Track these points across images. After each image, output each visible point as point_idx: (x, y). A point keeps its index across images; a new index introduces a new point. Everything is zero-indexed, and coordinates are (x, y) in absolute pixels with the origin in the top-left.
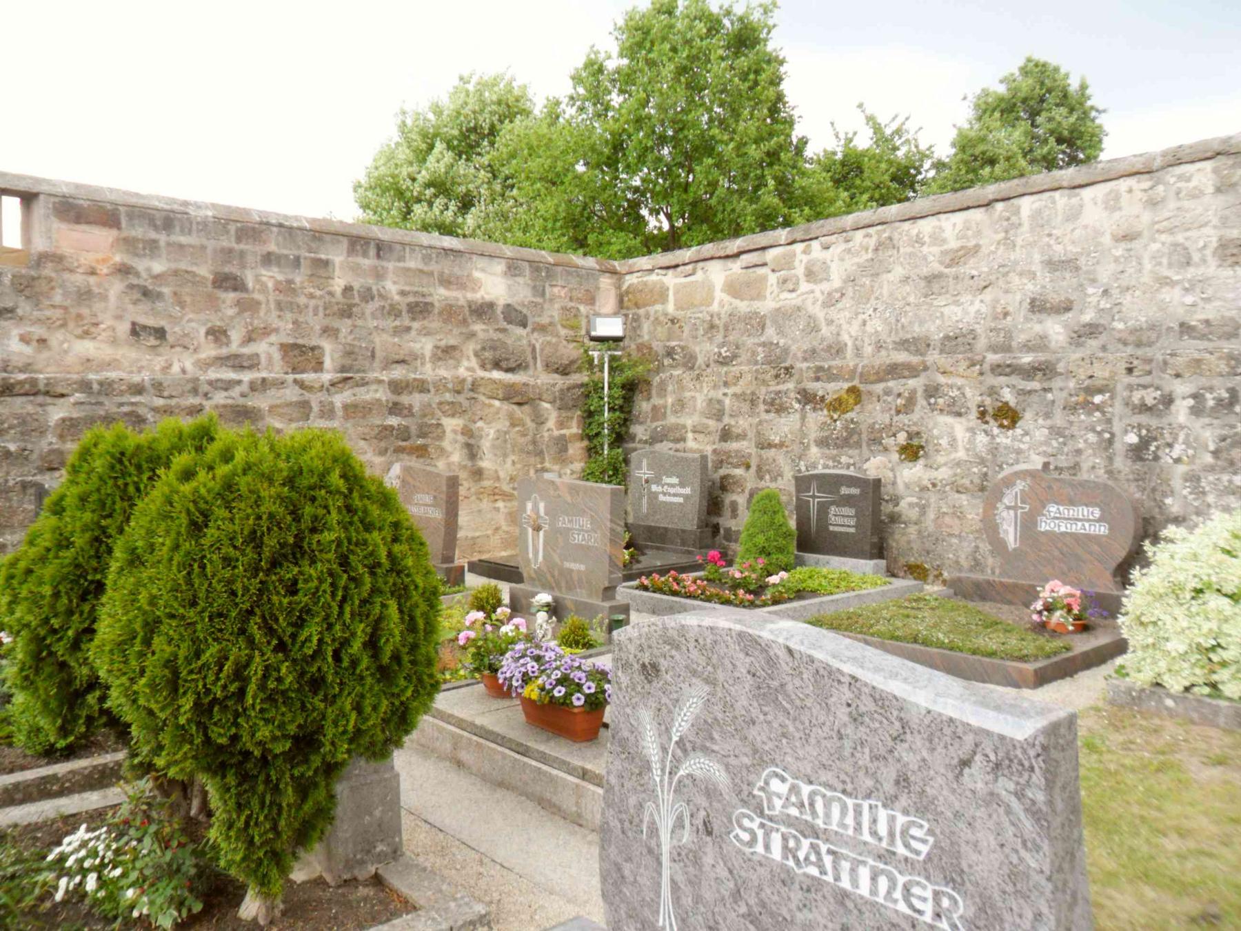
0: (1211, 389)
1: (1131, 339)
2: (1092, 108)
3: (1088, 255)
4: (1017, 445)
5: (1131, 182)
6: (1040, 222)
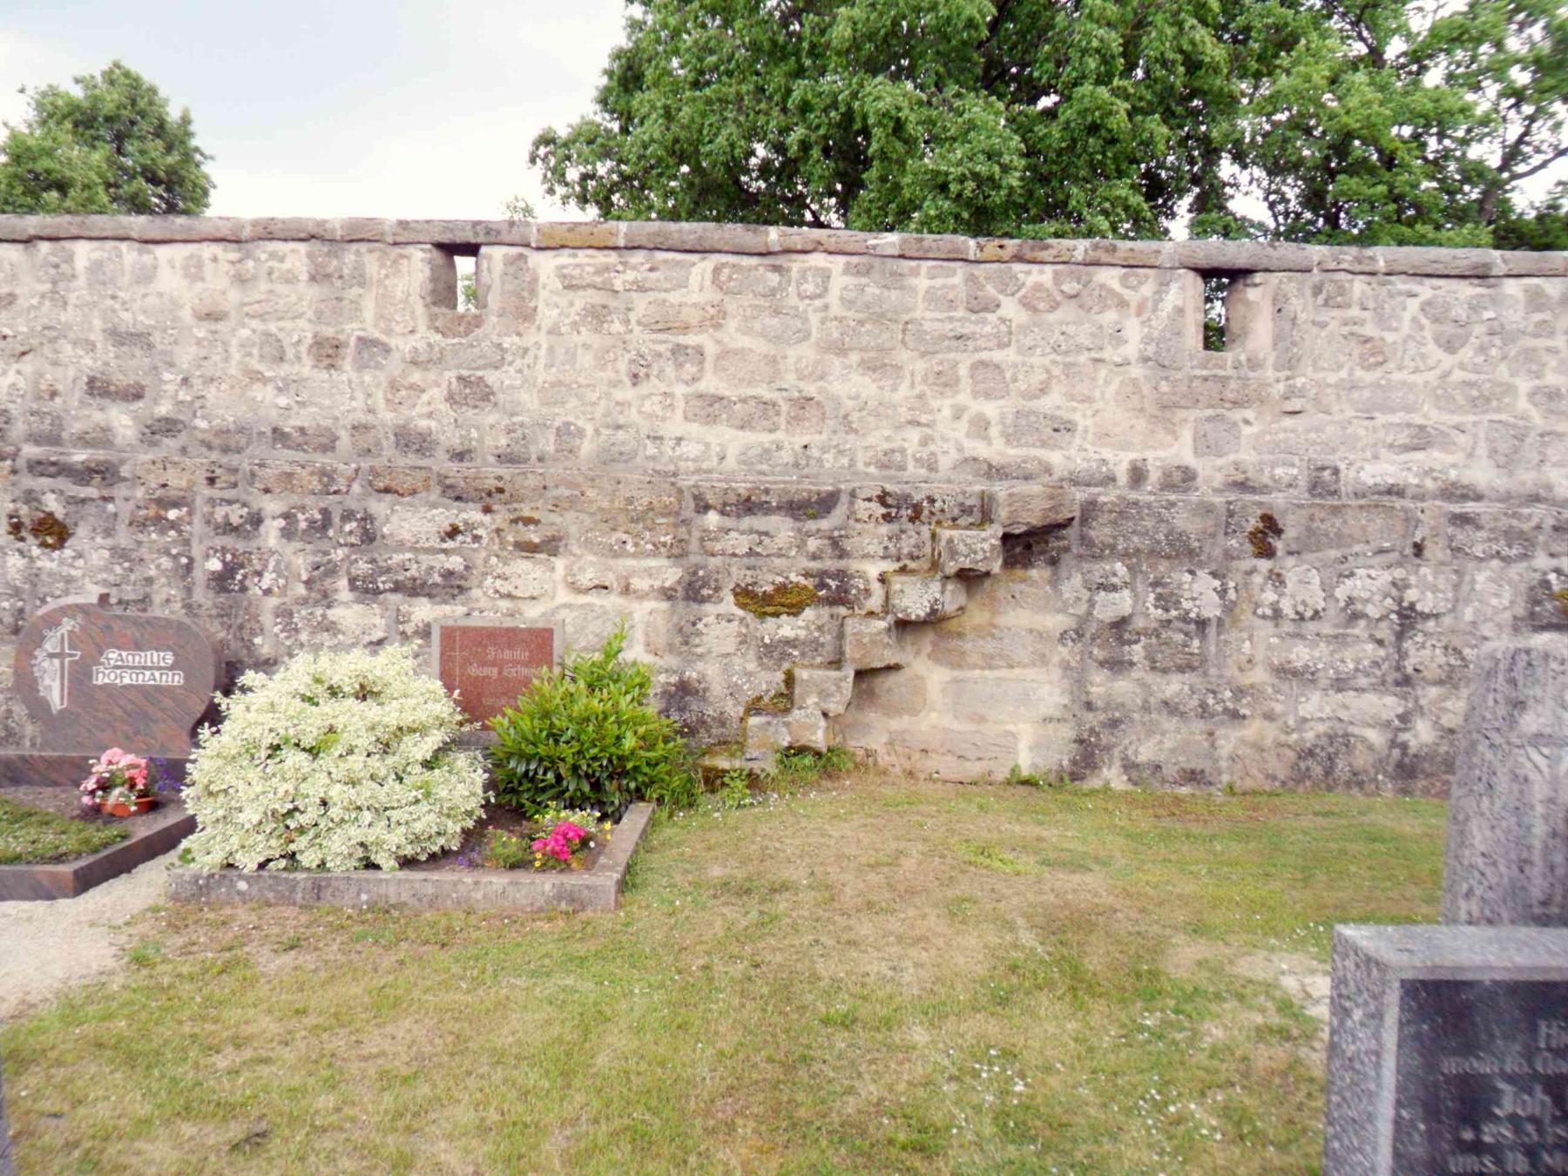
0: (303, 509)
1: (217, 442)
2: (197, 150)
3: (164, 331)
4: (65, 570)
5: (216, 249)
6: (101, 277)
